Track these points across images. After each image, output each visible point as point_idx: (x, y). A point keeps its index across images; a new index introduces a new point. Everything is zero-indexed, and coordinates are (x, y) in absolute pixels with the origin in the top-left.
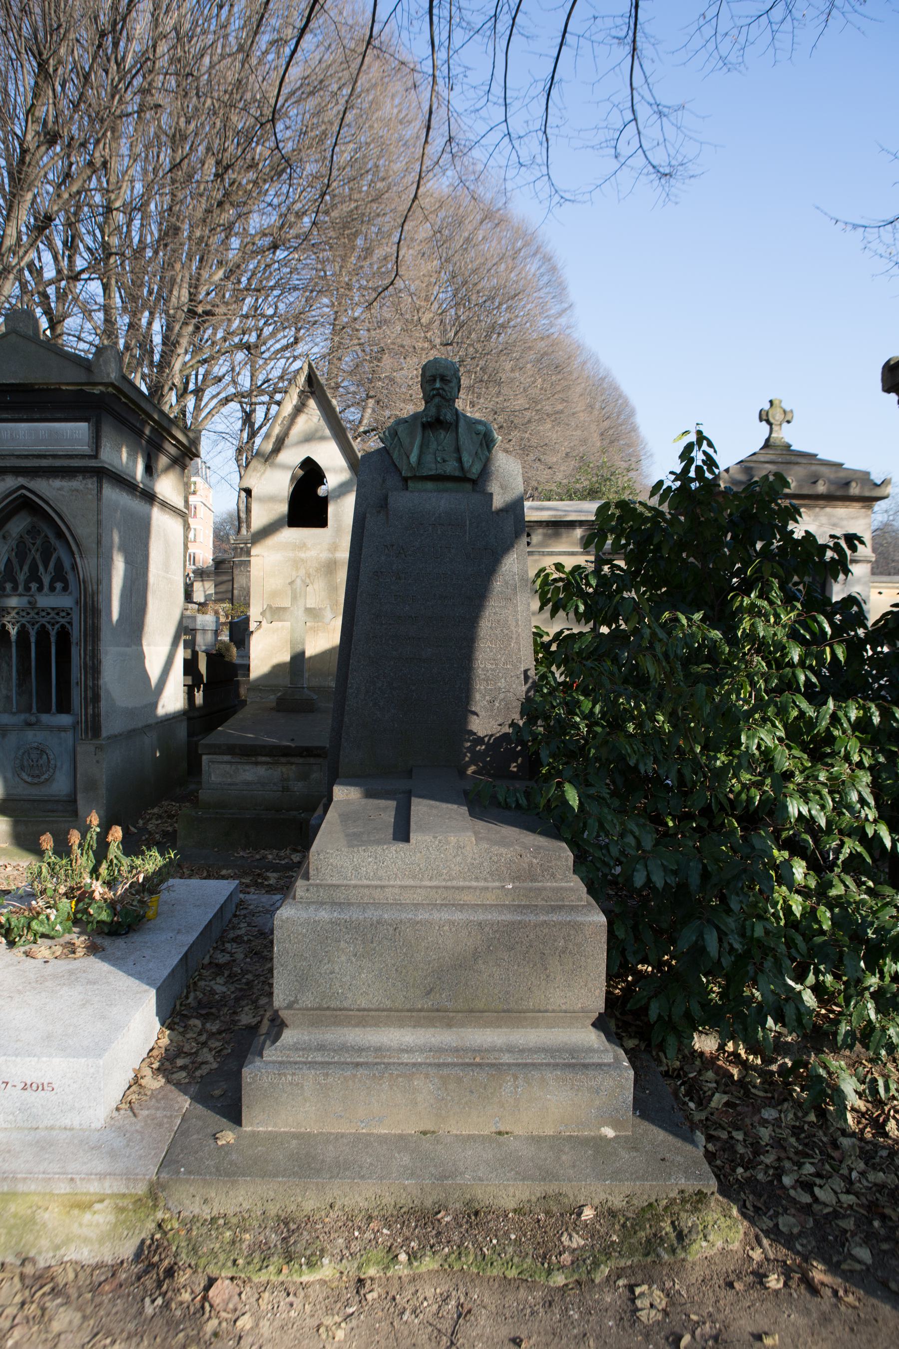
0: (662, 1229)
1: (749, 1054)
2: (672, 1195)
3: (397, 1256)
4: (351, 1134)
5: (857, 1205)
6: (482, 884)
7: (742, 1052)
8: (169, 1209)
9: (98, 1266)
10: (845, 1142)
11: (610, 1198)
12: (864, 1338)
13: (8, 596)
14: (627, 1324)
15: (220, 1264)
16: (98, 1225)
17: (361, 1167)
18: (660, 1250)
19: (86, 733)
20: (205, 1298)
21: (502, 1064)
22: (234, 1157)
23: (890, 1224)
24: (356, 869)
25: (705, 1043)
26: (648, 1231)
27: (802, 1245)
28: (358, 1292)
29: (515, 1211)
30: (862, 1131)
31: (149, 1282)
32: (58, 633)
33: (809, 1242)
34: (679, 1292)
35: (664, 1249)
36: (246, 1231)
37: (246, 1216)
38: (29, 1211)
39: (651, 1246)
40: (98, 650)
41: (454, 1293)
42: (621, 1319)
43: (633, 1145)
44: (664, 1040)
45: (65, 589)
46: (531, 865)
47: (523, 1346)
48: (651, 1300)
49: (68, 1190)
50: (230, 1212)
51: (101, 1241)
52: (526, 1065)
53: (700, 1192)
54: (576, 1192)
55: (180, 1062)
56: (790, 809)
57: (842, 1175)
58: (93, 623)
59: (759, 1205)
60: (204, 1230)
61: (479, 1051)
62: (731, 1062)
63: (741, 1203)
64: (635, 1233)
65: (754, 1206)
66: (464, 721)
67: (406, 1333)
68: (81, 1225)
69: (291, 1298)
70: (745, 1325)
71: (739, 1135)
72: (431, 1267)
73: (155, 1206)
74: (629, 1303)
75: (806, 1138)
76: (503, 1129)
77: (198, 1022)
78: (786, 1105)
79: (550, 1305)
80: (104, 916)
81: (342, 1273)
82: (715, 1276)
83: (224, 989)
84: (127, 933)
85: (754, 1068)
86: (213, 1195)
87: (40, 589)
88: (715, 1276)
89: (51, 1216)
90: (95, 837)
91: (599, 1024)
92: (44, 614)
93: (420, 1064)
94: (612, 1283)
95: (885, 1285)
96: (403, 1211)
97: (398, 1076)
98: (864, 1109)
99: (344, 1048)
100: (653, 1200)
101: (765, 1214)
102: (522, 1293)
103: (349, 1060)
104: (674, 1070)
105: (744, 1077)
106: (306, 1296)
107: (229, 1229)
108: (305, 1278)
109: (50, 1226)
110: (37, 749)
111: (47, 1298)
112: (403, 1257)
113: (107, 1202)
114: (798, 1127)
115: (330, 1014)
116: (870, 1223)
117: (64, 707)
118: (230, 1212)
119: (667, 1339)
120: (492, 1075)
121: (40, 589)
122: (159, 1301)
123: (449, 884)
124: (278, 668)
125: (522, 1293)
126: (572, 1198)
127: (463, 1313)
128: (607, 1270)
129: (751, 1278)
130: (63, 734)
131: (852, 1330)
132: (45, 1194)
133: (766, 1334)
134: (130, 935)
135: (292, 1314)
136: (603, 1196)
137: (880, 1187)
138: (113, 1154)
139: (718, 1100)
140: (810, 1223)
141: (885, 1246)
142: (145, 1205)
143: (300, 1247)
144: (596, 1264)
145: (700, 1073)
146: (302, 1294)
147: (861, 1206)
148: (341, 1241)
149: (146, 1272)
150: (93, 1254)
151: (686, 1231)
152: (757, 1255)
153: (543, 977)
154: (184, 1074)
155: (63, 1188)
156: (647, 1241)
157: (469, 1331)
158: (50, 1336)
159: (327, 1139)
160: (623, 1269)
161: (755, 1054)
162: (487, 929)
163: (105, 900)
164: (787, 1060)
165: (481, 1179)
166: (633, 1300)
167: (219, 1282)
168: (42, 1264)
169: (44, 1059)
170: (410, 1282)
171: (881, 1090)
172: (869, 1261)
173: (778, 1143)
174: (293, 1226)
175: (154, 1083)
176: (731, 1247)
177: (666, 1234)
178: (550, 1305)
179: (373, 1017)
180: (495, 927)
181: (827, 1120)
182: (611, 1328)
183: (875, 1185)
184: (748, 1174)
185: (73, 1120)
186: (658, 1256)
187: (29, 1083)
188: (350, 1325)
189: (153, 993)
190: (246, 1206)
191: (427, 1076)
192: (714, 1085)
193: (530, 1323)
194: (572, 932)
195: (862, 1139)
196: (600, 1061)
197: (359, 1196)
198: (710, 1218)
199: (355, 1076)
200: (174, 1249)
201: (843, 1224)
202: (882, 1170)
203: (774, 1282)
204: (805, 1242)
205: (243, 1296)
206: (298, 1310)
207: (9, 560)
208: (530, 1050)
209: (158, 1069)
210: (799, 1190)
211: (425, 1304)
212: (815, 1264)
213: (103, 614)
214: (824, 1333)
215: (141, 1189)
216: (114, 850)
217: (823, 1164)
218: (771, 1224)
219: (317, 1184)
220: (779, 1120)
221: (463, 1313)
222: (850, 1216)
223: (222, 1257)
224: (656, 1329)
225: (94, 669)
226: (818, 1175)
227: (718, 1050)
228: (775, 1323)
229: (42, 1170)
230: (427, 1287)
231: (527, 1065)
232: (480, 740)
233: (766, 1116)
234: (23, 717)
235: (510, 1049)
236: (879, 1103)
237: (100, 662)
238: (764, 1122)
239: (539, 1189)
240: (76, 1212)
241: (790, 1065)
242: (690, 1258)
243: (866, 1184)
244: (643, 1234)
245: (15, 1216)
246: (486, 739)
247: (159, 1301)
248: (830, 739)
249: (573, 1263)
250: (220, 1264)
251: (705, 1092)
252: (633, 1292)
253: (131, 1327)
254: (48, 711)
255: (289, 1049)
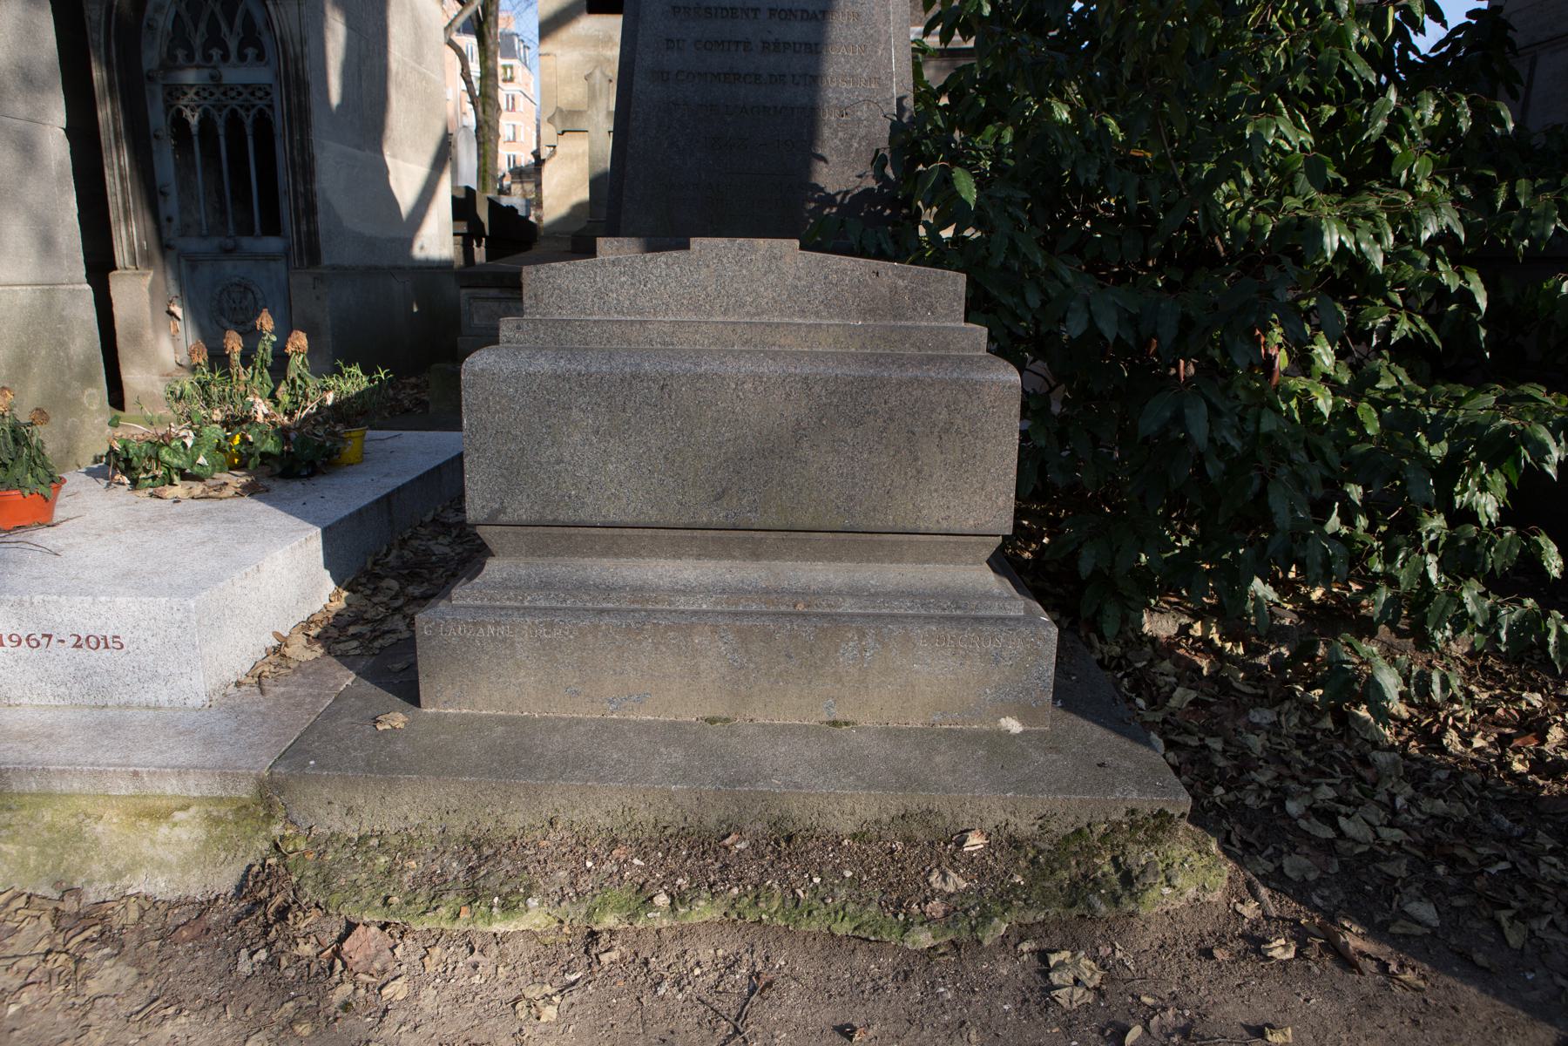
0: (1097, 867)
1: (1224, 641)
2: (1114, 817)
3: (651, 898)
4: (593, 720)
5: (1408, 842)
6: (812, 320)
7: (1215, 636)
8: (293, 823)
9: (178, 904)
10: (1381, 758)
11: (1012, 819)
12: (1437, 1034)
13: (182, 68)
14: (1034, 1009)
15: (362, 903)
16: (179, 842)
17: (602, 766)
18: (1094, 899)
19: (301, 259)
20: (337, 953)
21: (840, 615)
22: (399, 746)
23: (1463, 870)
24: (601, 295)
25: (1159, 625)
26: (1074, 871)
27: (1322, 898)
28: (586, 952)
29: (854, 836)
30: (1405, 744)
31: (251, 928)
32: (255, 121)
33: (1334, 893)
34: (1121, 962)
35: (1101, 896)
36: (411, 856)
37: (415, 834)
38: (73, 821)
39: (1077, 892)
40: (310, 141)
41: (747, 956)
42: (1025, 1000)
43: (1053, 744)
44: (1099, 611)
45: (260, 57)
46: (894, 290)
47: (856, 1038)
48: (1076, 975)
49: (131, 791)
50: (390, 829)
51: (185, 867)
52: (879, 616)
53: (1162, 813)
54: (957, 810)
55: (352, 630)
56: (1327, 239)
57: (1379, 803)
58: (300, 101)
59: (1251, 840)
60: (347, 853)
61: (804, 593)
62: (1197, 650)
63: (1223, 835)
64: (1052, 873)
65: (1242, 841)
66: (807, 169)
67: (661, 1014)
68: (153, 842)
69: (476, 957)
70: (1232, 1012)
71: (1216, 744)
72: (708, 917)
73: (269, 817)
74: (1039, 977)
75: (1317, 751)
76: (839, 717)
77: (395, 585)
78: (1287, 705)
79: (906, 978)
80: (270, 446)
81: (561, 922)
82: (1181, 940)
83: (447, 550)
84: (309, 476)
85: (1234, 659)
86: (360, 801)
87: (225, 57)
88: (1181, 940)
89: (108, 828)
90: (269, 350)
91: (1003, 561)
92: (234, 94)
93: (705, 612)
94: (1010, 947)
95: (1465, 958)
96: (668, 832)
97: (668, 628)
98: (1406, 715)
99: (582, 586)
100: (1082, 824)
101: (1260, 853)
102: (860, 959)
103: (589, 605)
104: (1112, 658)
105: (1217, 672)
106: (501, 955)
107: (386, 853)
108: (498, 927)
109: (106, 843)
110: (238, 285)
111: (90, 946)
112: (662, 900)
113: (193, 810)
114: (1305, 737)
115: (561, 531)
116: (1431, 868)
117: (272, 226)
118: (390, 829)
119: (1102, 1032)
120: (824, 630)
121: (225, 57)
122: (262, 955)
123: (756, 319)
124: (577, 208)
125: (860, 959)
126: (949, 818)
127: (758, 986)
128: (1004, 926)
129: (1240, 945)
130: (272, 265)
131: (1415, 1022)
132: (96, 796)
133: (1271, 1027)
134: (314, 480)
135: (476, 979)
136: (1000, 817)
137: (1442, 820)
138: (210, 742)
139: (1181, 697)
140: (1335, 867)
141: (1459, 902)
142: (253, 816)
143: (493, 881)
144: (986, 917)
145: (1151, 663)
146: (496, 951)
147: (1415, 844)
148: (562, 874)
149: (249, 912)
150: (173, 886)
151: (1137, 871)
152: (1249, 910)
153: (911, 472)
154: (355, 644)
155: (124, 787)
156: (1074, 884)
157: (765, 1013)
158: (79, 1001)
159: (552, 726)
160: (1029, 926)
161: (1235, 642)
162: (817, 389)
163: (274, 424)
164: (1283, 650)
165: (797, 786)
166: (1045, 972)
167: (361, 929)
168: (91, 897)
169: (103, 599)
170: (674, 938)
171: (1436, 687)
172: (1436, 923)
173: (1276, 756)
174: (487, 851)
175: (300, 651)
176: (1209, 897)
177: (1104, 875)
178: (906, 978)
179: (629, 538)
180: (831, 386)
181: (1350, 728)
182: (1007, 1013)
183: (1432, 816)
184: (1231, 797)
185: (161, 694)
186: (1090, 907)
187: (84, 637)
188: (569, 1000)
189: (316, 533)
190: (414, 819)
191: (715, 629)
192: (1173, 680)
193: (870, 1005)
194: (962, 397)
195: (1405, 755)
196: (1002, 613)
197: (598, 808)
198: (1175, 853)
199: (597, 627)
200: (294, 879)
201: (1388, 868)
202: (1440, 796)
203: (1280, 950)
204: (1327, 893)
205: (398, 951)
206: (487, 976)
207: (177, 15)
208: (887, 594)
209: (318, 638)
210: (1313, 820)
211: (697, 971)
212: (1346, 924)
213: (313, 89)
214: (1369, 1027)
215: (245, 791)
216: (296, 364)
217: (1349, 787)
218: (1270, 867)
219: (526, 787)
220: (1276, 725)
221: (758, 986)
222: (1396, 857)
223: (366, 894)
224: (1083, 1016)
225: (305, 169)
226: (1340, 800)
227: (1177, 635)
228: (1284, 1010)
229: (90, 760)
230: (701, 947)
231: (880, 617)
232: (829, 200)
233: (1257, 719)
234: (216, 241)
235: (855, 592)
236: (1431, 708)
237: (312, 158)
238: (1254, 728)
239: (894, 805)
240: (146, 823)
241: (1287, 654)
242: (1143, 912)
243: (1418, 815)
244: (1066, 874)
245: (51, 827)
246: (839, 198)
247: (262, 955)
248: (1383, 158)
249: (946, 914)
250: (362, 903)
251: (1159, 688)
252: (1045, 961)
253: (213, 991)
254: (250, 232)
255: (494, 588)
